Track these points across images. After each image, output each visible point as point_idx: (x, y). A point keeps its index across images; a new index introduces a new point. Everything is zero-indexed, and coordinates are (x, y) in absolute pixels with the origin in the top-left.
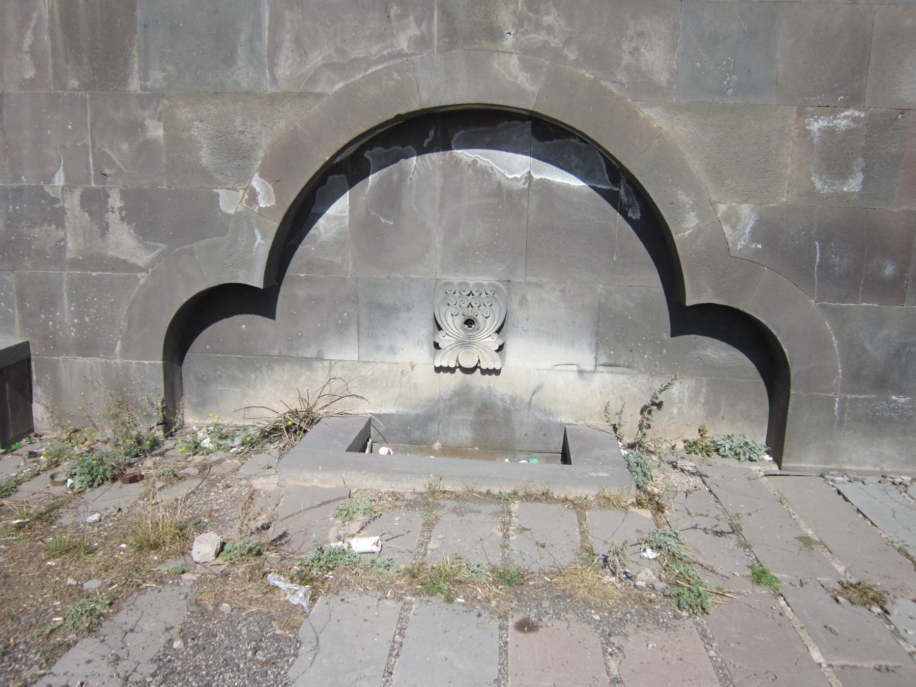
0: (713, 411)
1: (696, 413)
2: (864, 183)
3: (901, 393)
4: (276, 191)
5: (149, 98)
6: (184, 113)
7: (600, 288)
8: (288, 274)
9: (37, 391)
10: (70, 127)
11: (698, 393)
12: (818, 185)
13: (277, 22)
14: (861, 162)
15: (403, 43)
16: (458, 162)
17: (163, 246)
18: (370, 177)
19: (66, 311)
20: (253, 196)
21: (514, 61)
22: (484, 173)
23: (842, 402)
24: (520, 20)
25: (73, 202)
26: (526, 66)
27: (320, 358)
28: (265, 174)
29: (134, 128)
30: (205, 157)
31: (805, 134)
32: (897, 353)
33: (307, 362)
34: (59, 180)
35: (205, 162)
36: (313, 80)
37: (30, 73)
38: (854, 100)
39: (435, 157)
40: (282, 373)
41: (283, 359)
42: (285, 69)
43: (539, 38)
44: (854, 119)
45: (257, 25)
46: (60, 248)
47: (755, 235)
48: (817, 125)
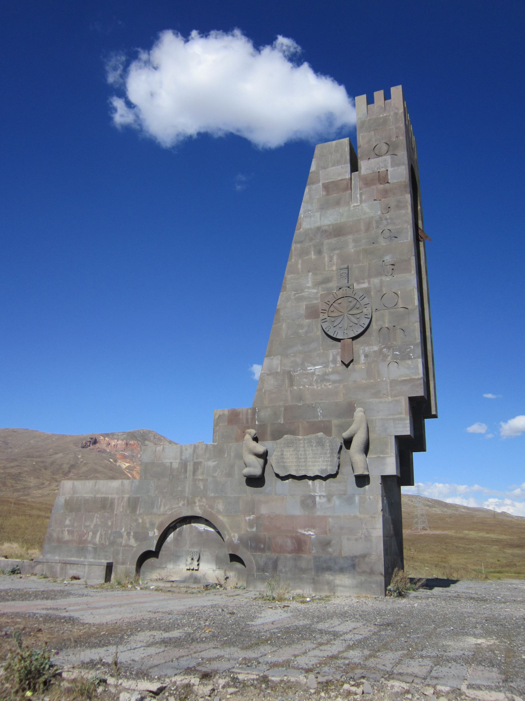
0: (239, 579)
1: (235, 580)
2: (256, 529)
3: (267, 572)
4: (159, 532)
5: (140, 514)
6: (145, 518)
7: (217, 552)
8: (162, 549)
9: (113, 573)
10: (411, 355)
11: (235, 575)
12: (248, 530)
13: (161, 501)
14: (255, 525)
15: (181, 505)
16: (192, 526)
17: (138, 543)
18: (177, 529)
19: (120, 556)
20: (155, 533)
21: (198, 508)
22: (196, 528)
23: (256, 574)
24: (199, 501)
25: (125, 534)
26: (200, 509)
27: (166, 567)
28: (157, 529)
29: (137, 520)
30: (148, 526)
31: (245, 520)
32: (266, 564)
33: (163, 568)
34: (123, 530)
35: (147, 526)
36: (166, 511)
37: (122, 510)
38: (253, 513)
39: (188, 525)
40: (158, 571)
41: (159, 568)
42: (162, 510)
43: (202, 504)
44: (254, 517)
45: (158, 502)
46: (121, 543)
47: (238, 540)
48: (247, 518)
